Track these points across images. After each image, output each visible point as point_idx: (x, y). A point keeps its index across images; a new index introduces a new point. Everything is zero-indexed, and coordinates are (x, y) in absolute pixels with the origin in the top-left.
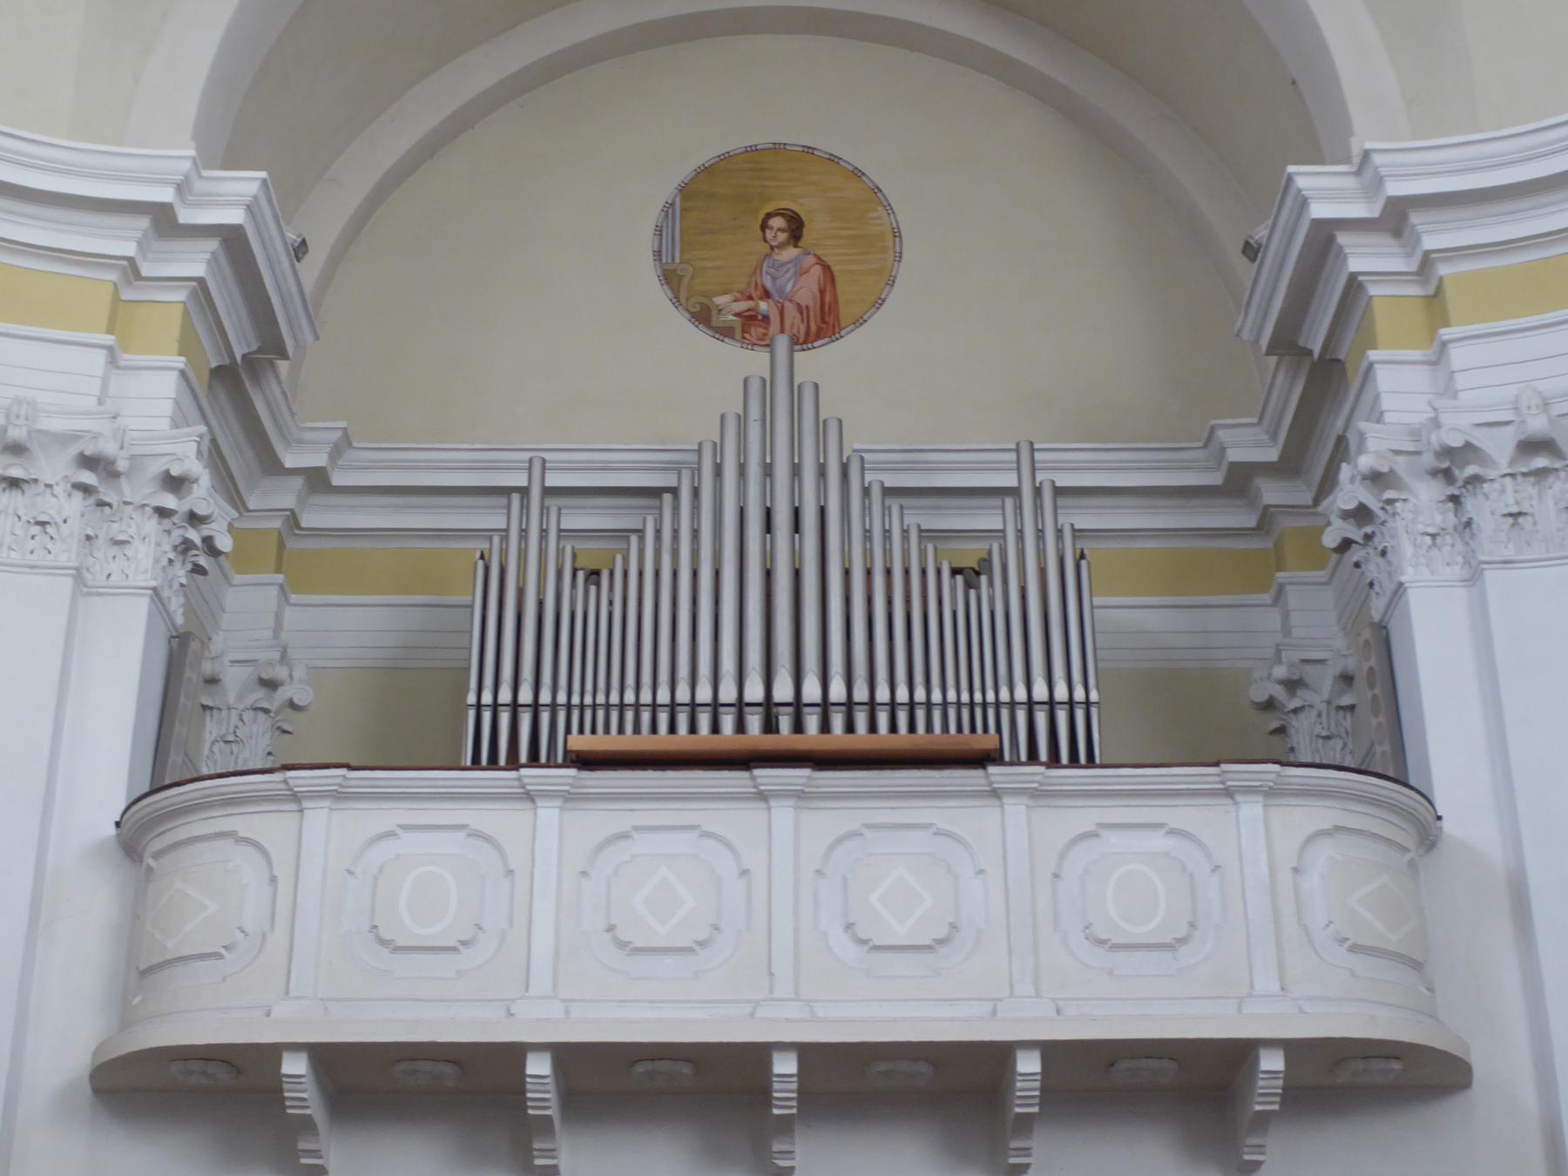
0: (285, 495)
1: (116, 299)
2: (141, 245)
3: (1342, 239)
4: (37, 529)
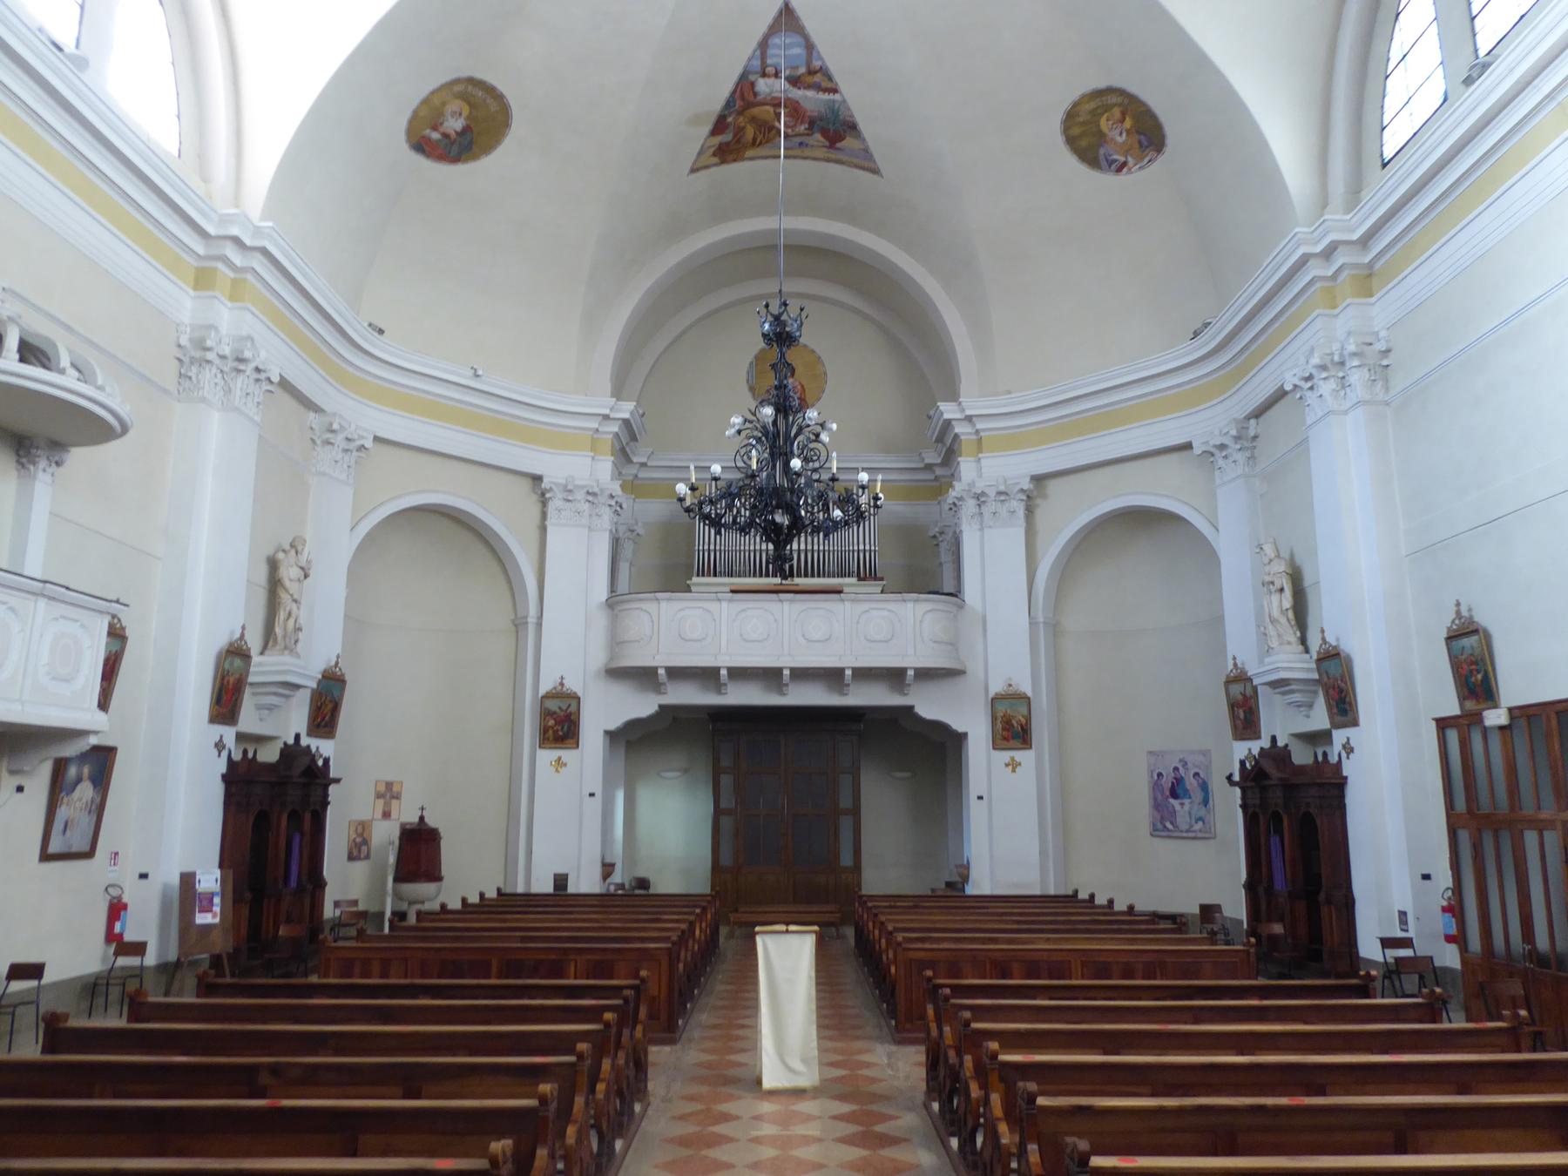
0: (632, 470)
1: (593, 438)
2: (600, 424)
3: (953, 423)
4: (576, 514)
